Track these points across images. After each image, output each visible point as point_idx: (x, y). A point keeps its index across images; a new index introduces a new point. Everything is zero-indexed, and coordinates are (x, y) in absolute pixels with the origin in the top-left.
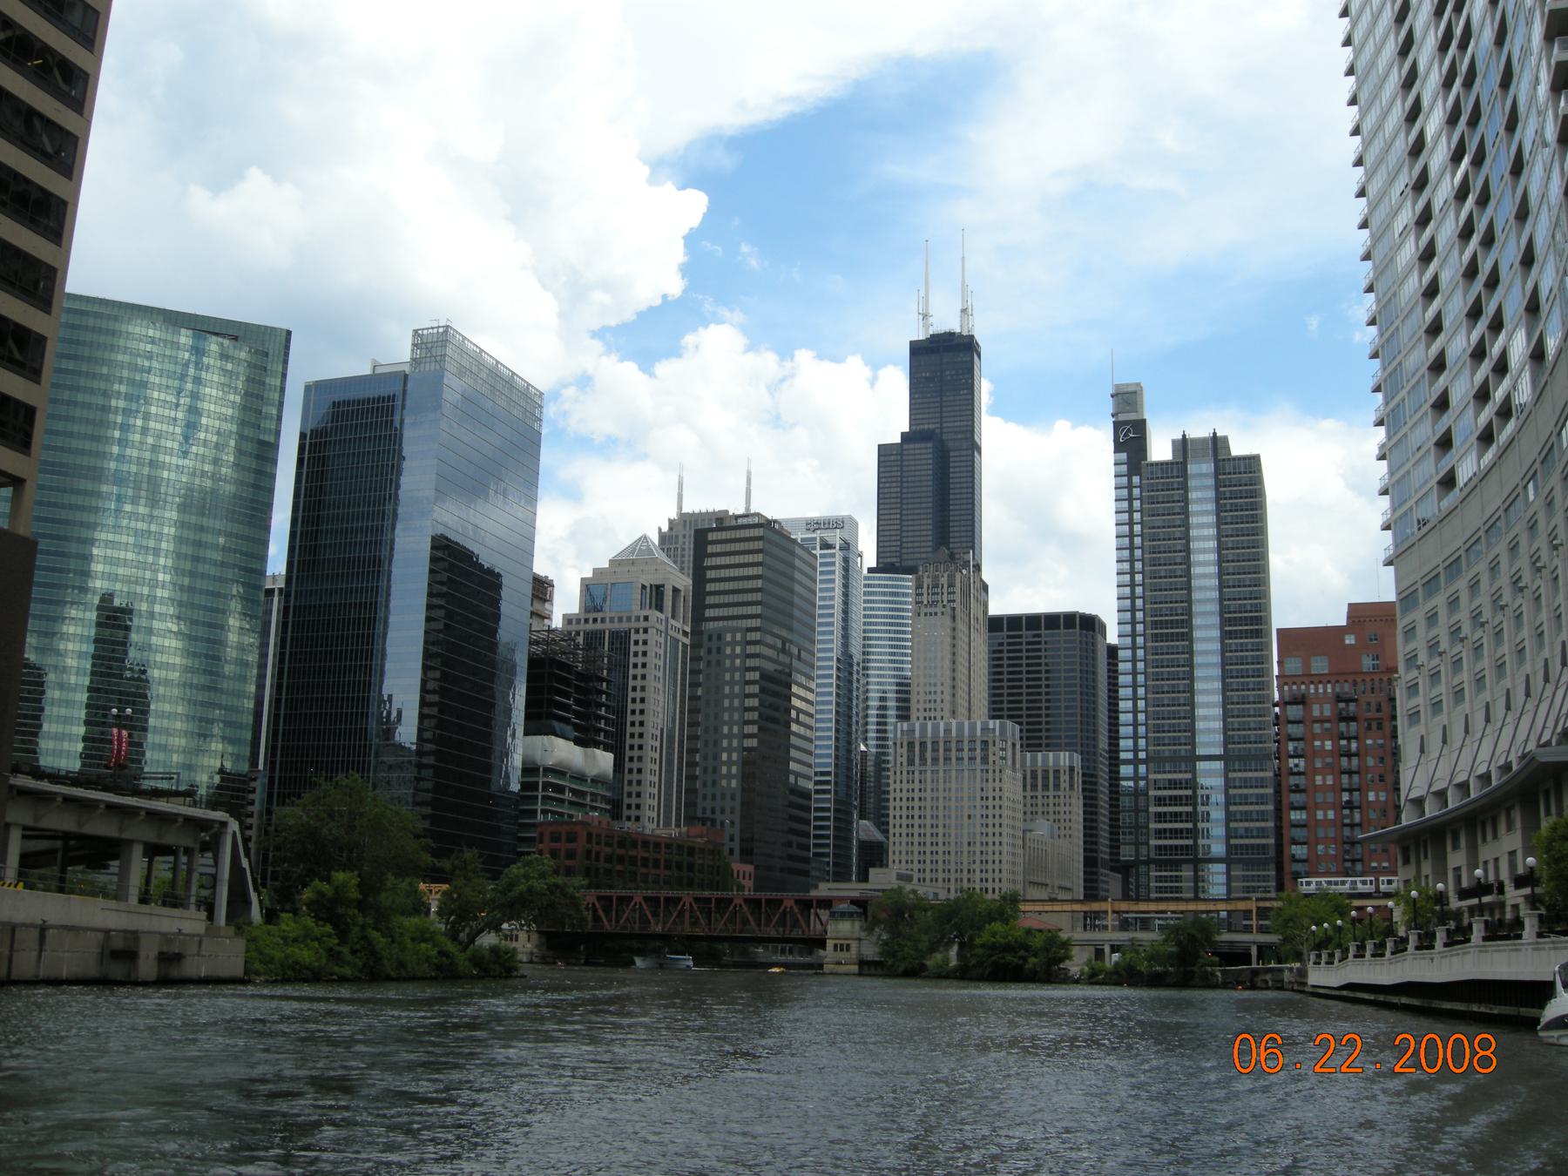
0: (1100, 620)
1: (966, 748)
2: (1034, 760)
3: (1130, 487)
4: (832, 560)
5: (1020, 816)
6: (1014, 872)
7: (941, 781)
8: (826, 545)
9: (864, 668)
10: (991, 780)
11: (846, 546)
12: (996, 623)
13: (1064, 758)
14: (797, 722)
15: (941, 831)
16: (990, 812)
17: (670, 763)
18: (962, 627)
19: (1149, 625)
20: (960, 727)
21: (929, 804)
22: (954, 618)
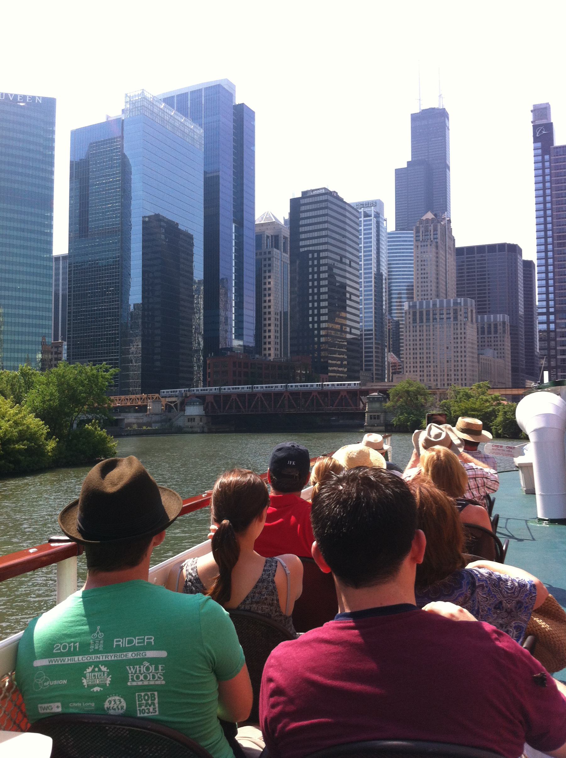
0: (519, 247)
1: (445, 312)
2: (483, 319)
3: (543, 162)
4: (370, 223)
5: (476, 347)
6: (473, 375)
7: (431, 330)
8: (367, 215)
9: (389, 279)
10: (459, 328)
11: (378, 215)
12: (460, 251)
13: (500, 317)
14: (350, 299)
15: (432, 355)
16: (459, 345)
17: (286, 325)
18: (441, 252)
19: (555, 238)
20: (441, 302)
21: (425, 342)
22: (437, 247)
